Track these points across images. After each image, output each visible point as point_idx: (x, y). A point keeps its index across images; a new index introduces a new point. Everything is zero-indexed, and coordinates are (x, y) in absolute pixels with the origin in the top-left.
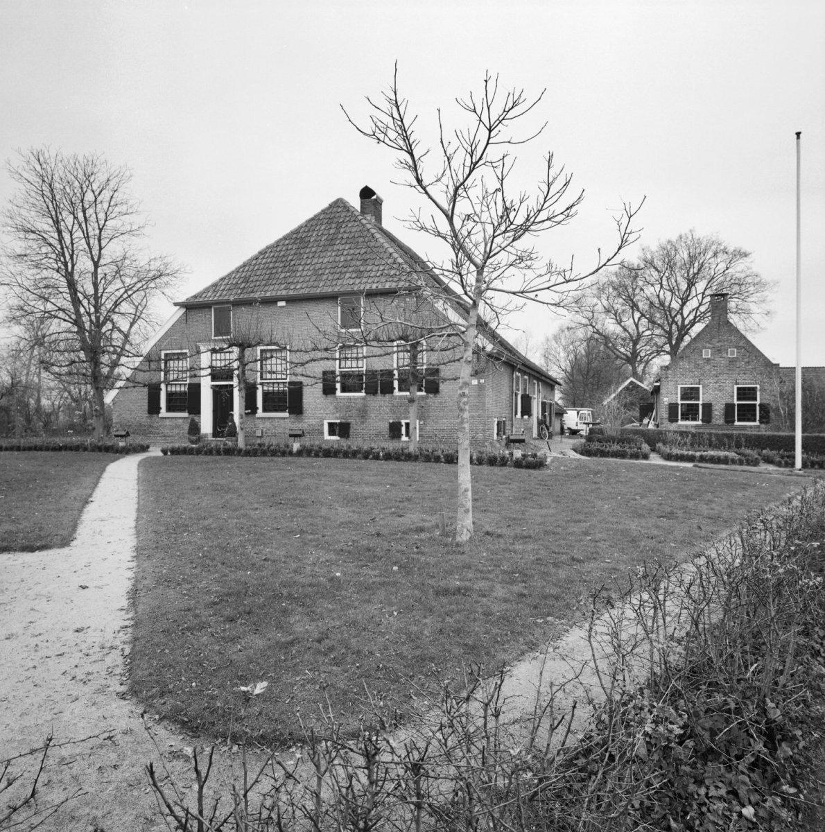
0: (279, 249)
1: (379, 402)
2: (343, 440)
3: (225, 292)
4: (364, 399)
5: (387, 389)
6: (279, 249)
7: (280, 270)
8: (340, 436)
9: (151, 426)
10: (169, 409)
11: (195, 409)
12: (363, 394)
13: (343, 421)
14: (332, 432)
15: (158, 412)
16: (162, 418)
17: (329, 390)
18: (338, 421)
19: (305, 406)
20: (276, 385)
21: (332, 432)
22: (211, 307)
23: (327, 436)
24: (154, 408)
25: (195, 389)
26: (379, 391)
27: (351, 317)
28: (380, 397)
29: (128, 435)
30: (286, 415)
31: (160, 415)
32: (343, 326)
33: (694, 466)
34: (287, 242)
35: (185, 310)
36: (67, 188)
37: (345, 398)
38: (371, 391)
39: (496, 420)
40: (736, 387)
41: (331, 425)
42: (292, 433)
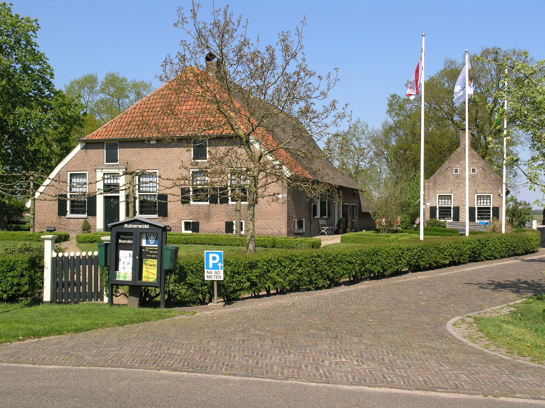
0: (150, 102)
1: (219, 207)
2: (195, 233)
3: (114, 133)
4: (209, 206)
5: (225, 201)
6: (150, 102)
7: (152, 118)
8: (193, 231)
9: (60, 224)
10: (72, 212)
11: (92, 212)
12: (208, 203)
13: (195, 221)
14: (186, 229)
15: (65, 215)
16: (67, 218)
17: (185, 200)
18: (191, 221)
19: (169, 211)
20: (152, 197)
21: (186, 229)
22: (103, 143)
23: (184, 231)
24: (62, 212)
25: (92, 200)
26: (219, 202)
27: (200, 153)
28: (219, 205)
29: (55, 230)
30: (156, 216)
31: (67, 216)
32: (194, 159)
33: (342, 241)
34: (156, 97)
35: (85, 144)
36: (390, 321)
37: (196, 205)
38: (213, 201)
39: (296, 220)
40: (476, 195)
41: (186, 223)
42: (48, 229)
